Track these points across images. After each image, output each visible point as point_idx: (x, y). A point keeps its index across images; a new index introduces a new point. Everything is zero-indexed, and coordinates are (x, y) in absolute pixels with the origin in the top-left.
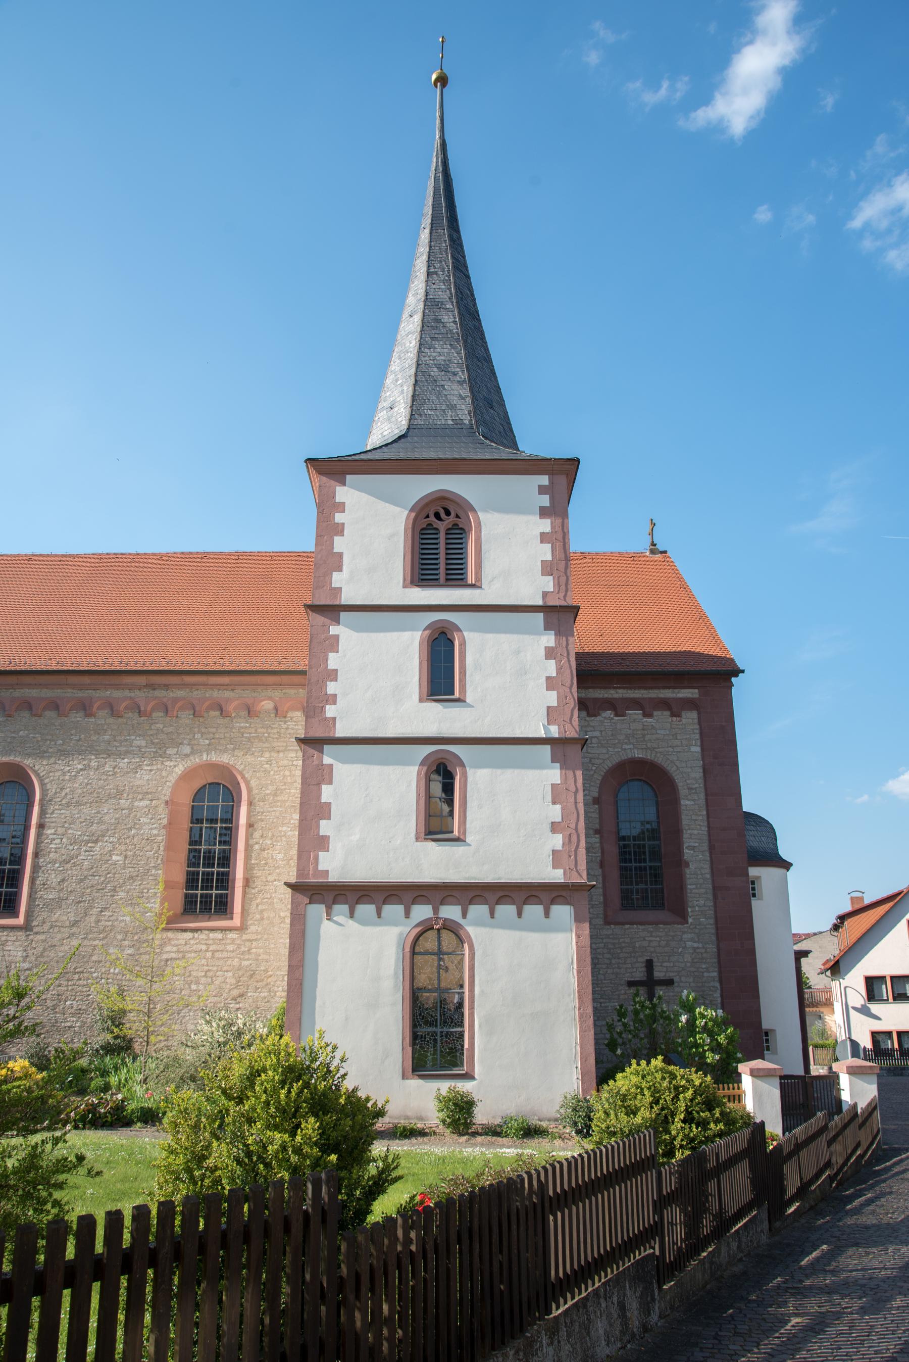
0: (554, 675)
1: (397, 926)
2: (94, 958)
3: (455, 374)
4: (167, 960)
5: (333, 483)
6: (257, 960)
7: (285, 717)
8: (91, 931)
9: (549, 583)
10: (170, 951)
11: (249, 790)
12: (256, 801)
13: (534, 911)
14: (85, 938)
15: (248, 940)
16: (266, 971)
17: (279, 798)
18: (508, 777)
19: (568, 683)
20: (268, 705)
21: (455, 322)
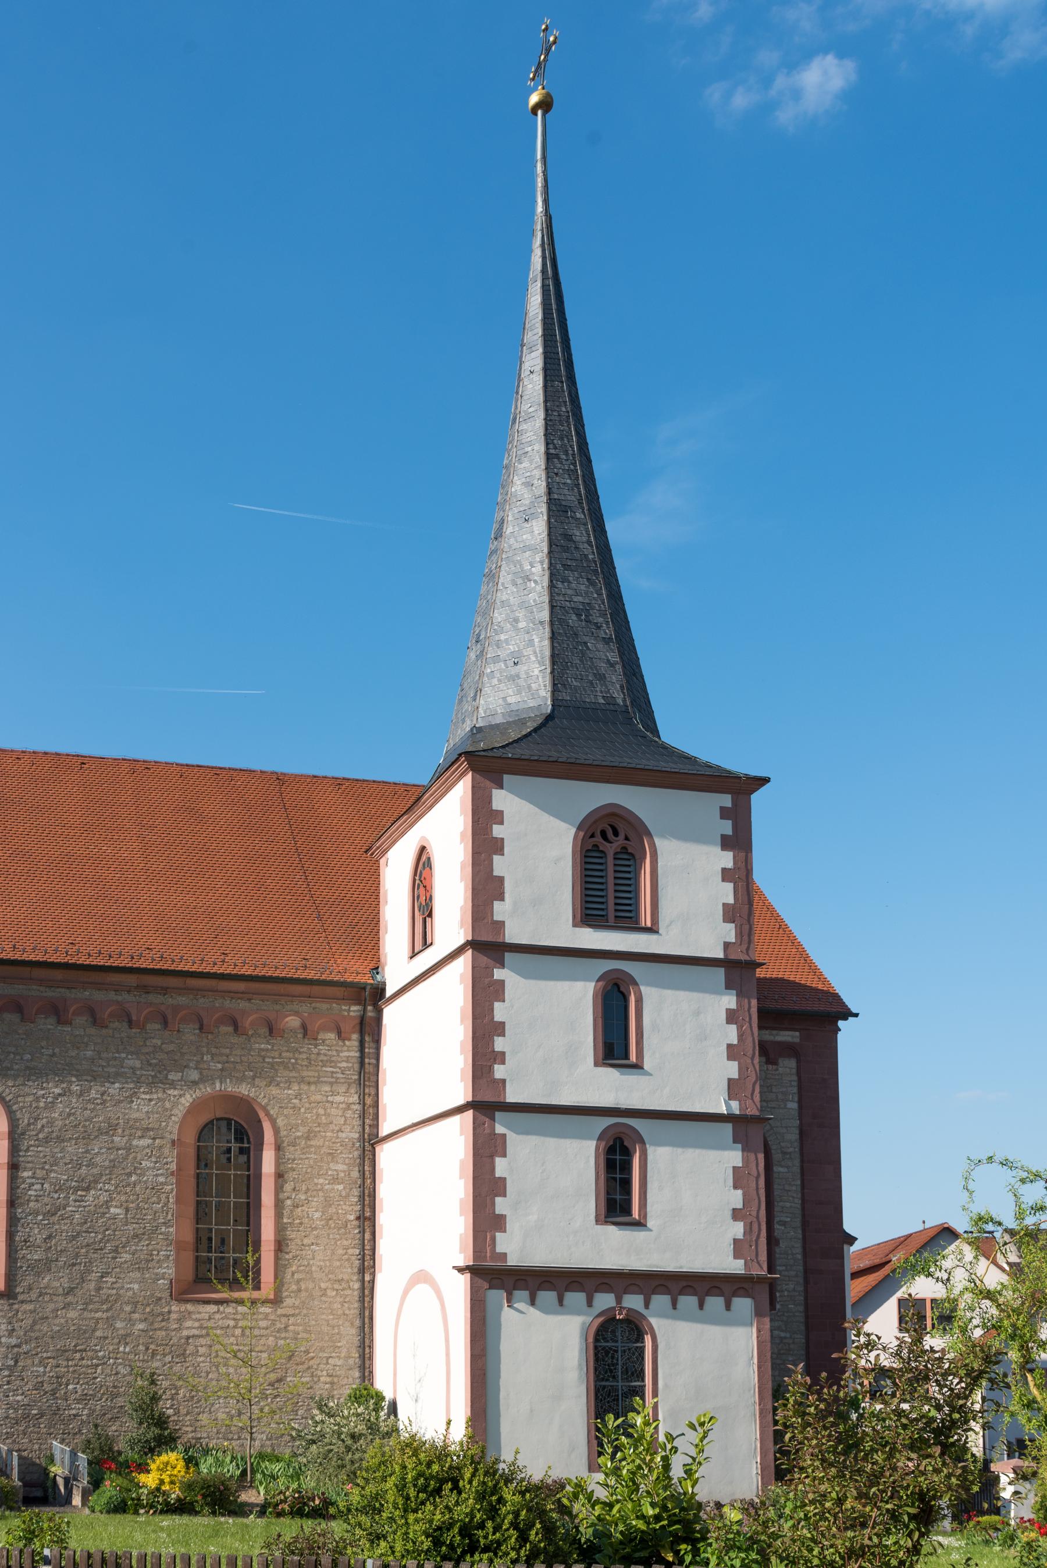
0: (735, 1042)
1: (579, 1315)
2: (99, 1334)
4: (188, 1338)
5: (488, 783)
6: (296, 1339)
7: (316, 1039)
8: (91, 1300)
9: (729, 932)
11: (276, 1131)
12: (285, 1144)
13: (715, 1303)
14: (84, 1309)
15: (285, 1315)
16: (307, 1352)
17: (312, 1143)
18: (691, 1155)
19: (750, 1053)
20: (293, 1022)
21: (589, 543)
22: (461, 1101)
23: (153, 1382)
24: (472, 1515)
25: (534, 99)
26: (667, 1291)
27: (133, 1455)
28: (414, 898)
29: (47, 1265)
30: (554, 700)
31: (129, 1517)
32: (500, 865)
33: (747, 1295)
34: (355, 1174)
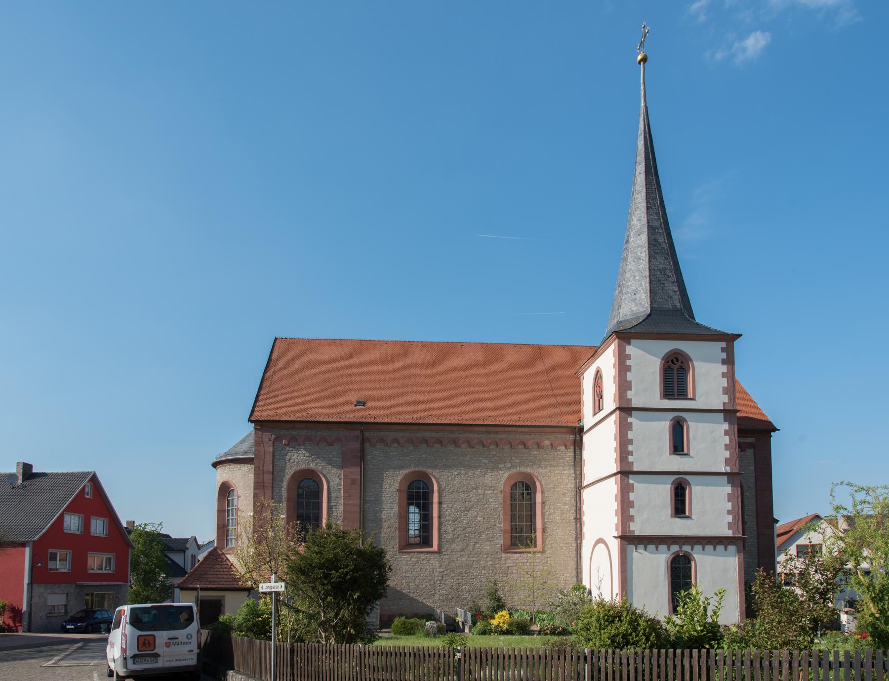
3: (669, 277)
9: (725, 399)
10: (509, 563)
11: (542, 486)
20: (547, 443)
22: (615, 471)
23: (495, 584)
24: (627, 630)
25: (639, 57)
26: (700, 544)
27: (488, 613)
28: (595, 391)
29: (454, 540)
30: (651, 308)
31: (487, 636)
32: (629, 376)
33: (734, 544)
34: (573, 501)
